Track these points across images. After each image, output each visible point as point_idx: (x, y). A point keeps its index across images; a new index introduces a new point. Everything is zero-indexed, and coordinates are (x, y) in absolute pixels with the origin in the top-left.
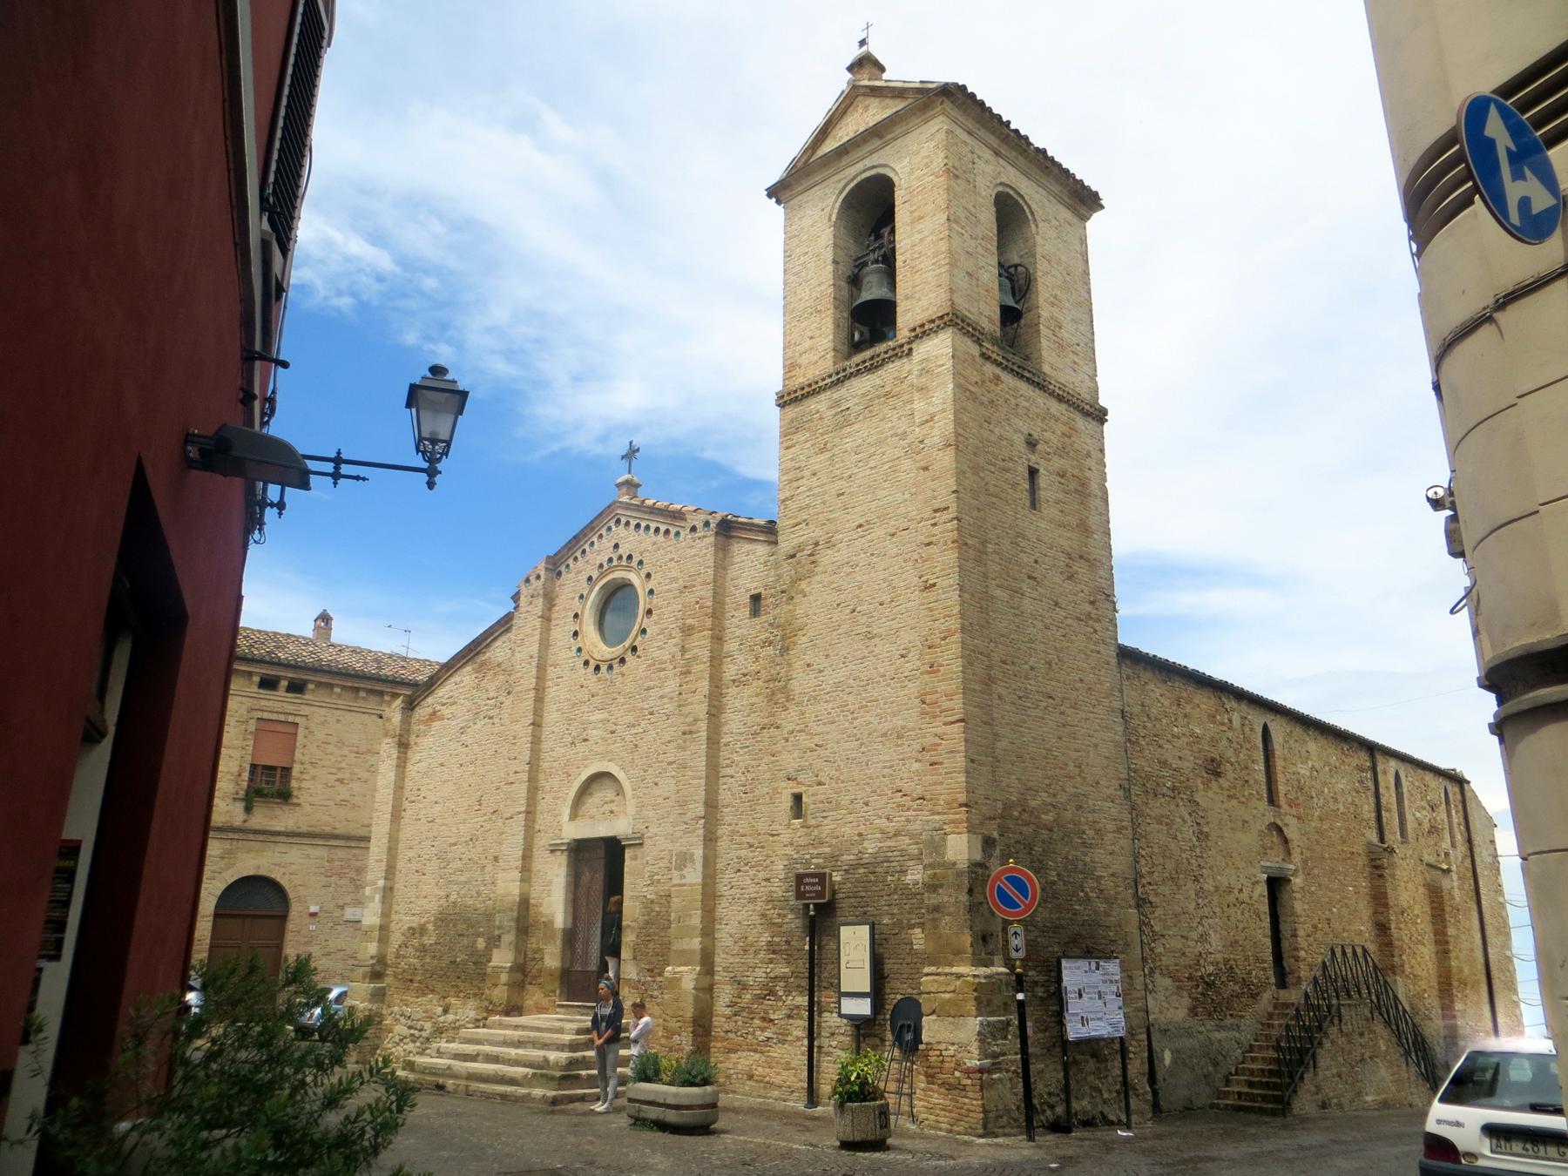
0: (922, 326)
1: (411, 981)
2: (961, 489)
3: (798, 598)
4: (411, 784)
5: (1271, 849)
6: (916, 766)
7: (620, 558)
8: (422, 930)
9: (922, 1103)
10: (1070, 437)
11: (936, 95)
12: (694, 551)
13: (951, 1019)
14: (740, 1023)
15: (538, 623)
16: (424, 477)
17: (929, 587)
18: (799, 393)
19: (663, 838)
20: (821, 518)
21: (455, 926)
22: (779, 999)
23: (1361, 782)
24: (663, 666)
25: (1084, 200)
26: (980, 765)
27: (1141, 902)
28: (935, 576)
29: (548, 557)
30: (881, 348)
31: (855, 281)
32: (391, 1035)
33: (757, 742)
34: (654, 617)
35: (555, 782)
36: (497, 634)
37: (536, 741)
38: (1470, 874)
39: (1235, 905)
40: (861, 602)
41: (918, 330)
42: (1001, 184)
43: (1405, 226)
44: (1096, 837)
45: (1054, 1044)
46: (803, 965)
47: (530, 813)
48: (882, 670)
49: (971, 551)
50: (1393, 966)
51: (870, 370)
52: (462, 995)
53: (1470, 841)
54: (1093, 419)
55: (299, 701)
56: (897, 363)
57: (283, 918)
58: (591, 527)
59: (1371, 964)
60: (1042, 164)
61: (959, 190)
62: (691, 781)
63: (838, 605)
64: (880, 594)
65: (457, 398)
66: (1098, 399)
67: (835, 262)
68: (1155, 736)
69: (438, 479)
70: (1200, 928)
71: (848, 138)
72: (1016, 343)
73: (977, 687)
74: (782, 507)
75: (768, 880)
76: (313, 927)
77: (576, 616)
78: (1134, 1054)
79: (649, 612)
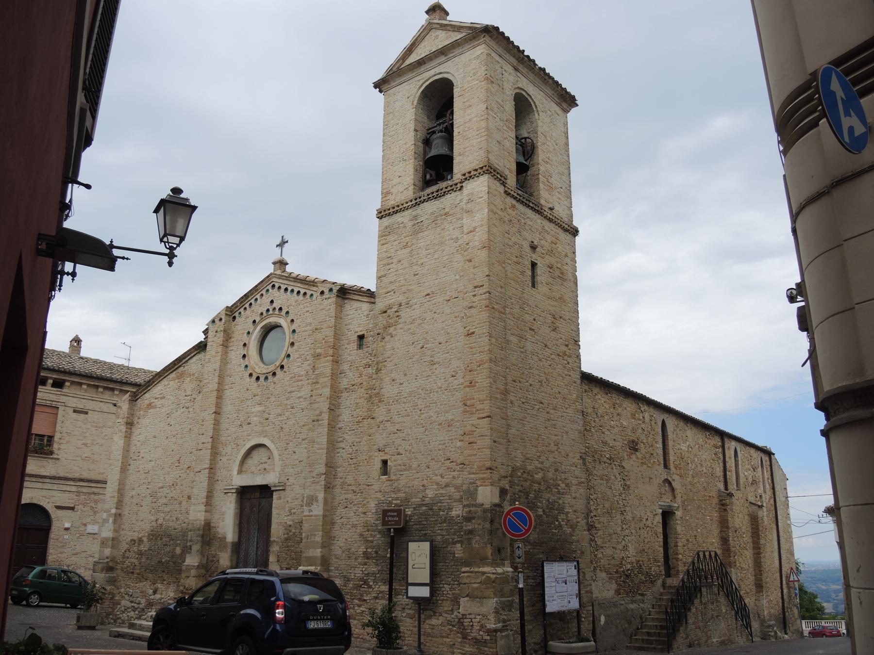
0: (470, 172)
1: (133, 573)
2: (491, 274)
3: (388, 338)
4: (134, 448)
5: (665, 494)
6: (459, 444)
7: (274, 309)
8: (141, 541)
9: (459, 651)
10: (555, 244)
12: (322, 307)
15: (220, 349)
16: (166, 259)
17: (470, 334)
18: (391, 210)
19: (298, 486)
20: (404, 289)
21: (161, 539)
22: (370, 587)
23: (716, 454)
24: (300, 378)
25: (567, 100)
26: (499, 444)
27: (590, 527)
29: (227, 307)
30: (443, 185)
32: (119, 606)
33: (360, 427)
34: (295, 347)
35: (228, 449)
36: (192, 355)
37: (217, 423)
38: (773, 508)
39: (643, 528)
40: (427, 342)
41: (467, 175)
43: (776, 135)
44: (566, 488)
46: (386, 568)
47: (212, 469)
48: (440, 385)
49: (496, 313)
50: (730, 562)
51: (436, 198)
52: (165, 582)
53: (773, 488)
54: (570, 233)
55: (59, 393)
56: (453, 194)
58: (255, 289)
59: (719, 562)
60: (543, 77)
61: (493, 90)
62: (317, 451)
63: (413, 343)
64: (439, 337)
65: (190, 210)
66: (572, 221)
67: (416, 130)
68: (600, 426)
69: (174, 260)
70: (624, 542)
71: (425, 54)
72: (525, 186)
73: (498, 396)
75: (365, 513)
76: (66, 537)
77: (245, 345)
78: (585, 618)
79: (292, 344)
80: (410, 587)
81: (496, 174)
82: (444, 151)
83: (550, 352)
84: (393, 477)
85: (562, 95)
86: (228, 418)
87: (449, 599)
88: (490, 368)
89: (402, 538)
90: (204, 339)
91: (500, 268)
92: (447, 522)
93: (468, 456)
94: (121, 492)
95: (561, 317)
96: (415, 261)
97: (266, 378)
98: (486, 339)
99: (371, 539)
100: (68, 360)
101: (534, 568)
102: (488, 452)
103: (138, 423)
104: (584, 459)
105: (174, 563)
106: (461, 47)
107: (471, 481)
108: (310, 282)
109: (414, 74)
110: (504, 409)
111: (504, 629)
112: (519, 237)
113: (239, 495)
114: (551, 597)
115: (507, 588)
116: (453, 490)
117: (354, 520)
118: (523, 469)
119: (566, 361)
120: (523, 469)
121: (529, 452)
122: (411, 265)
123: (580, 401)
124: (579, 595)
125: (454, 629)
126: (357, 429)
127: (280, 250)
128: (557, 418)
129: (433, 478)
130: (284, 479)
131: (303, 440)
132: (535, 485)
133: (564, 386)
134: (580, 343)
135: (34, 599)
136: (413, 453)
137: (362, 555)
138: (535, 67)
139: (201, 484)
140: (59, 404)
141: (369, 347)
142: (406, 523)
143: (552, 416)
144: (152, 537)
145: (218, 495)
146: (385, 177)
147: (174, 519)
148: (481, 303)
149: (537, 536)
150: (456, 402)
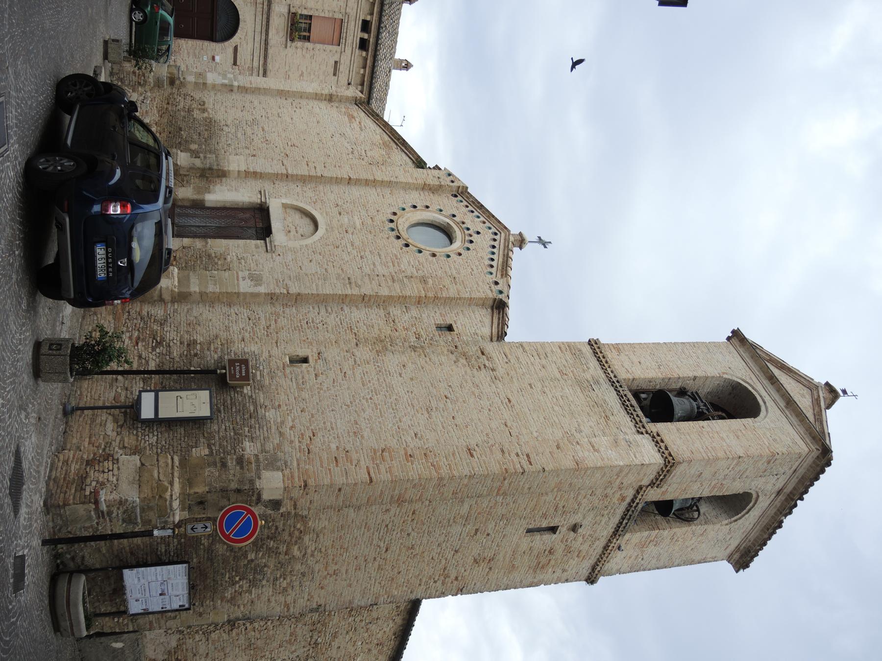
0: (662, 441)
1: (168, 103)
3: (453, 357)
6: (333, 446)
7: (471, 236)
8: (204, 111)
9: (71, 456)
10: (578, 556)
11: (823, 444)
12: (480, 283)
13: (137, 478)
14: (135, 321)
15: (420, 182)
18: (601, 355)
20: (512, 373)
22: (154, 349)
24: (396, 265)
26: (337, 496)
27: (232, 623)
28: (479, 456)
29: (467, 188)
31: (682, 392)
32: (131, 91)
34: (431, 258)
35: (310, 194)
37: (338, 181)
41: (658, 438)
42: (758, 496)
44: (281, 588)
45: (122, 560)
46: (179, 365)
48: (404, 419)
49: (499, 484)
51: (623, 404)
54: (590, 573)
55: (354, 46)
56: (631, 425)
57: (212, 38)
58: (490, 216)
60: (772, 526)
66: (603, 576)
67: (695, 378)
72: (643, 513)
73: (397, 492)
74: (517, 345)
76: (205, 58)
77: (427, 207)
78: (118, 622)
79: (434, 255)
80: (153, 394)
81: (664, 473)
83: (449, 558)
84: (288, 370)
85: (749, 551)
86: (344, 193)
87: (138, 444)
88: (431, 478)
89: (214, 384)
90: (429, 167)
91: (553, 485)
92: (236, 437)
93: (320, 458)
94: (257, 91)
95: (490, 568)
96: (547, 384)
97: (393, 230)
98: (466, 472)
99: (212, 349)
100: (388, 55)
101: (179, 552)
102: (327, 481)
103: (332, 106)
104: (316, 610)
105: (180, 143)
106: (799, 423)
107: (289, 462)
108: (506, 270)
109: (758, 373)
110: (380, 501)
111: (100, 514)
112: (587, 509)
113: (258, 206)
114: (143, 575)
115: (152, 516)
116: (276, 441)
117: (235, 328)
118: (305, 530)
119: (438, 579)
120: (305, 530)
121: (326, 537)
122: (542, 380)
123: (389, 600)
124: (146, 613)
125: (101, 452)
126: (342, 327)
127: (535, 240)
128: (368, 572)
129: (289, 417)
130: (279, 250)
131: (326, 269)
132: (285, 548)
133: (407, 577)
134: (459, 596)
135: (138, 16)
136: (319, 393)
137: (192, 338)
138: (783, 516)
139: (269, 166)
140: (343, 46)
141: (440, 337)
142: (232, 387)
143: (371, 564)
144: (208, 121)
145: (258, 185)
146: (636, 346)
147: (229, 142)
148: (509, 463)
149: (220, 553)
150: (385, 441)
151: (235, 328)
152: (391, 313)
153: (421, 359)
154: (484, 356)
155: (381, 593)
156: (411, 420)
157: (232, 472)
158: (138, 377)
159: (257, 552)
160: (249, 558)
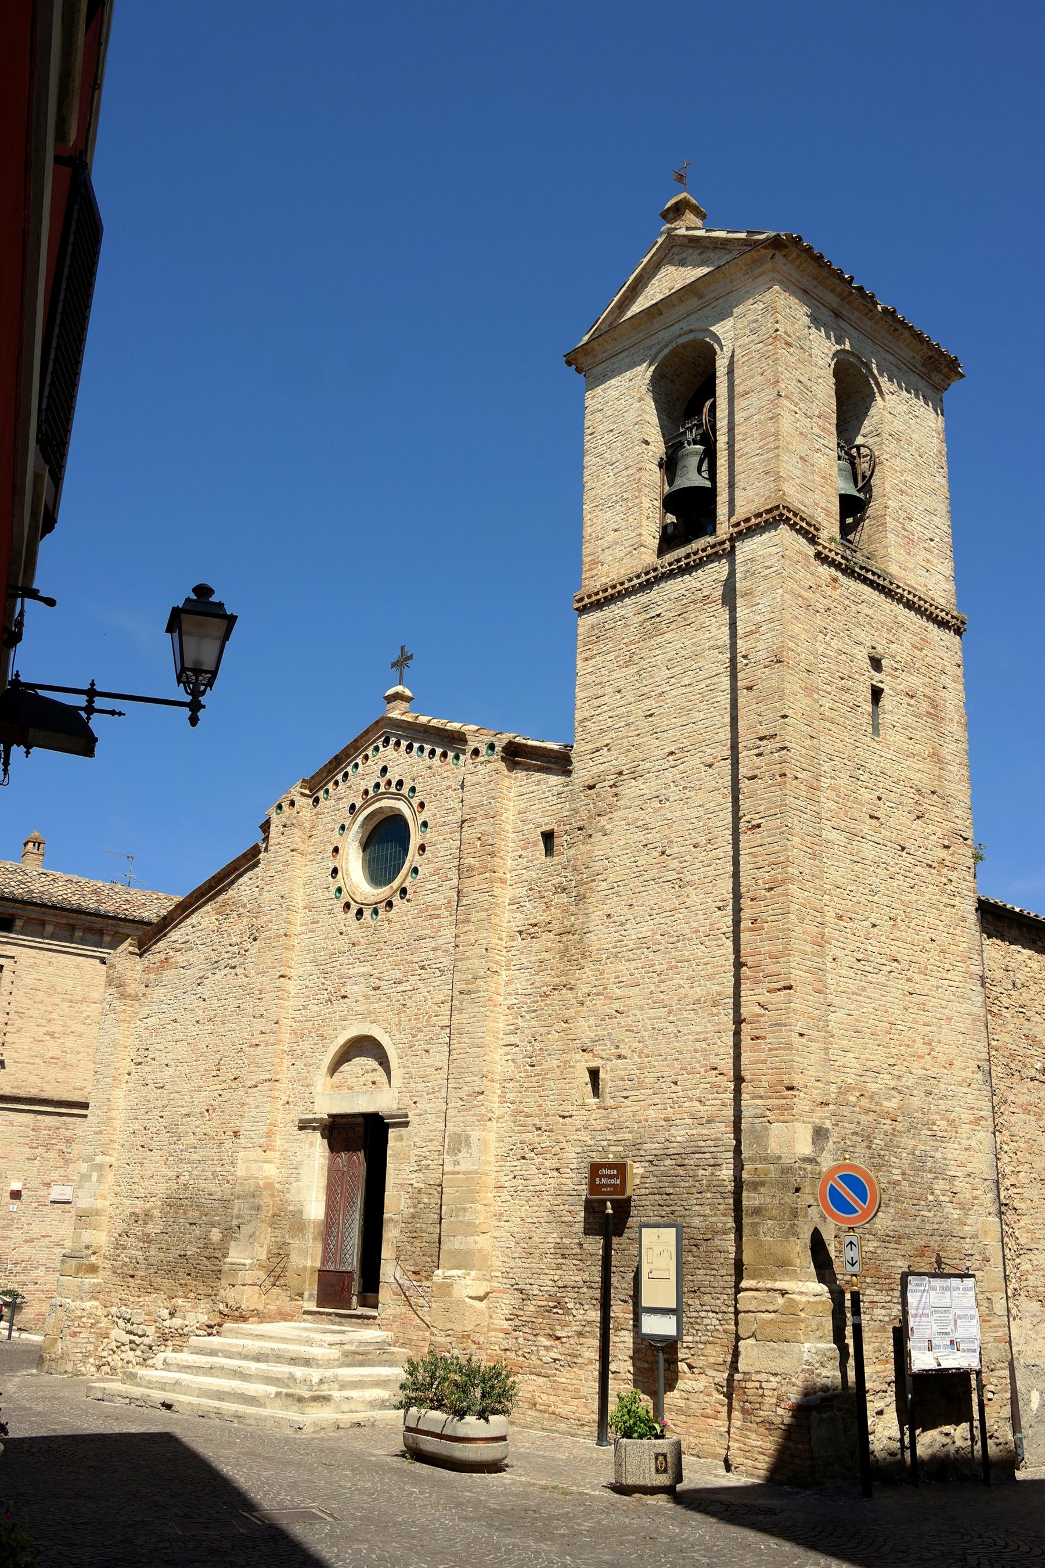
7: (389, 783)
16: (186, 712)
21: (185, 1213)
22: (568, 1312)
28: (760, 816)
33: (546, 1005)
34: (428, 854)
44: (949, 1129)
68: (1020, 1006)
69: (201, 714)
73: (808, 948)
77: (336, 850)
82: (700, 481)
83: (912, 861)
91: (808, 700)
100: (20, 878)
121: (871, 1057)
128: (929, 990)
143: (917, 986)
151: (536, 1182)
152: (520, 929)
153: (599, 889)
154: (597, 786)
155: (963, 970)
156: (696, 914)
157: (768, 1200)
158: (613, 1338)
159: (890, 1165)
160: (899, 1178)
